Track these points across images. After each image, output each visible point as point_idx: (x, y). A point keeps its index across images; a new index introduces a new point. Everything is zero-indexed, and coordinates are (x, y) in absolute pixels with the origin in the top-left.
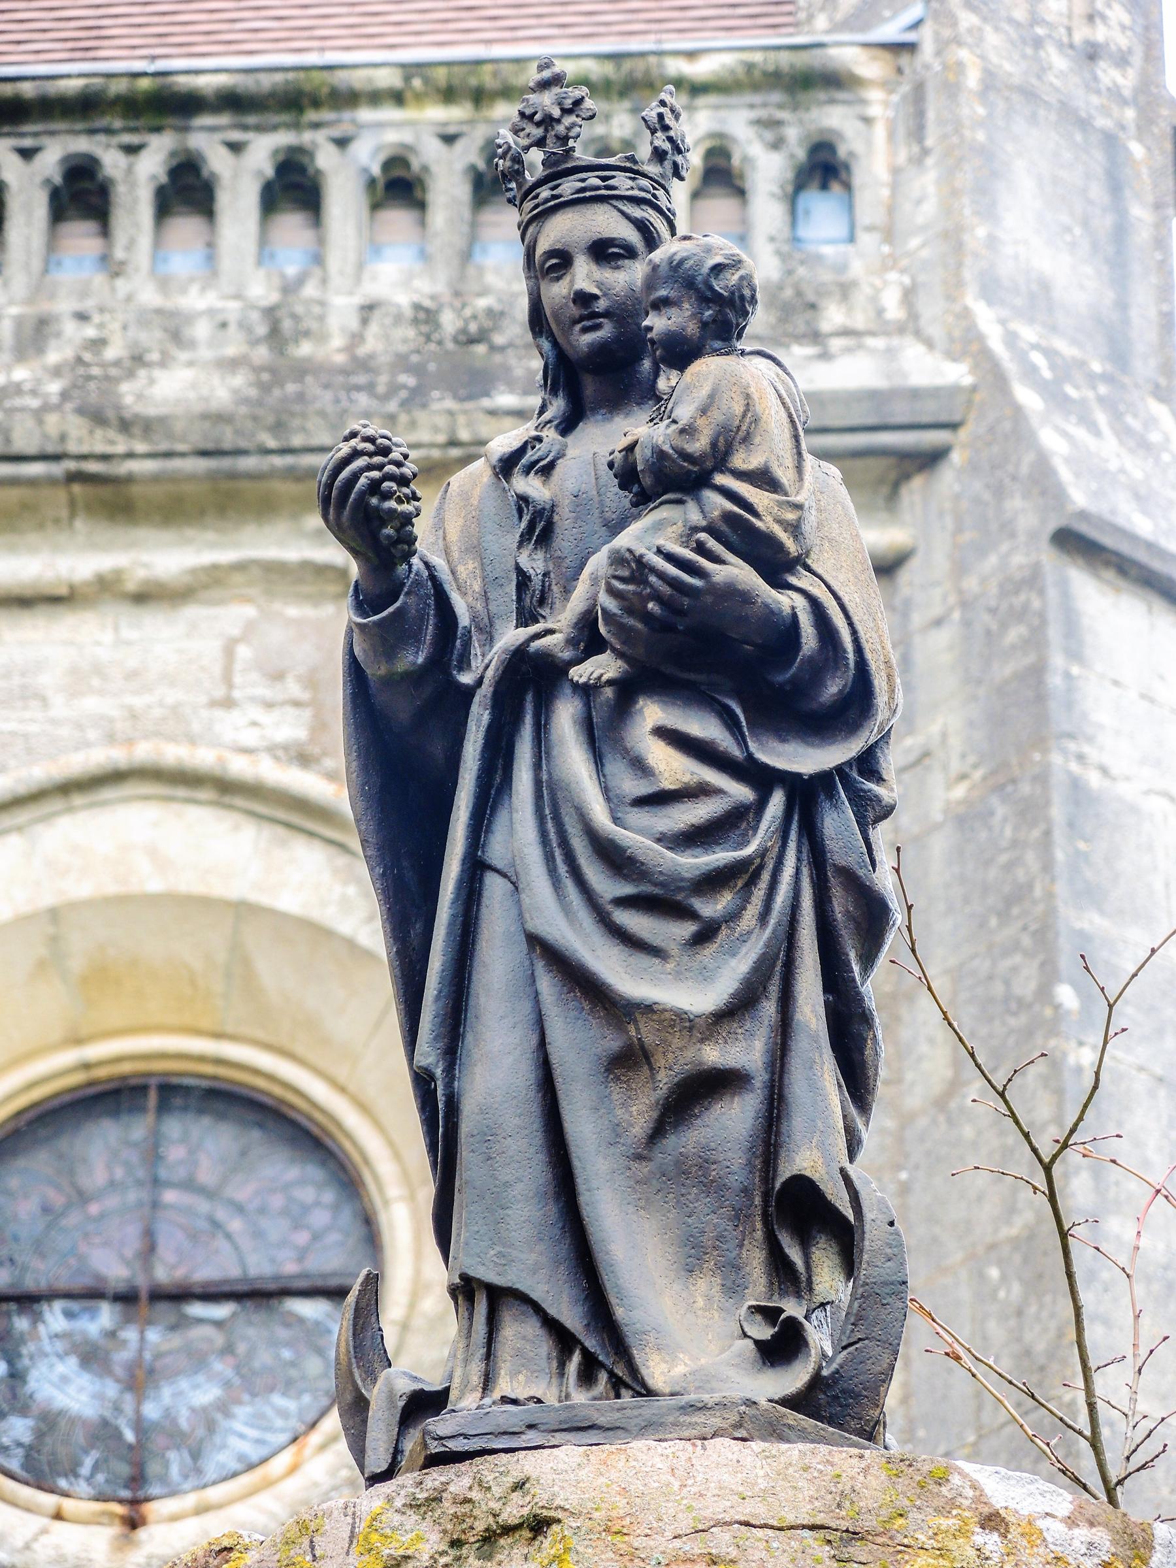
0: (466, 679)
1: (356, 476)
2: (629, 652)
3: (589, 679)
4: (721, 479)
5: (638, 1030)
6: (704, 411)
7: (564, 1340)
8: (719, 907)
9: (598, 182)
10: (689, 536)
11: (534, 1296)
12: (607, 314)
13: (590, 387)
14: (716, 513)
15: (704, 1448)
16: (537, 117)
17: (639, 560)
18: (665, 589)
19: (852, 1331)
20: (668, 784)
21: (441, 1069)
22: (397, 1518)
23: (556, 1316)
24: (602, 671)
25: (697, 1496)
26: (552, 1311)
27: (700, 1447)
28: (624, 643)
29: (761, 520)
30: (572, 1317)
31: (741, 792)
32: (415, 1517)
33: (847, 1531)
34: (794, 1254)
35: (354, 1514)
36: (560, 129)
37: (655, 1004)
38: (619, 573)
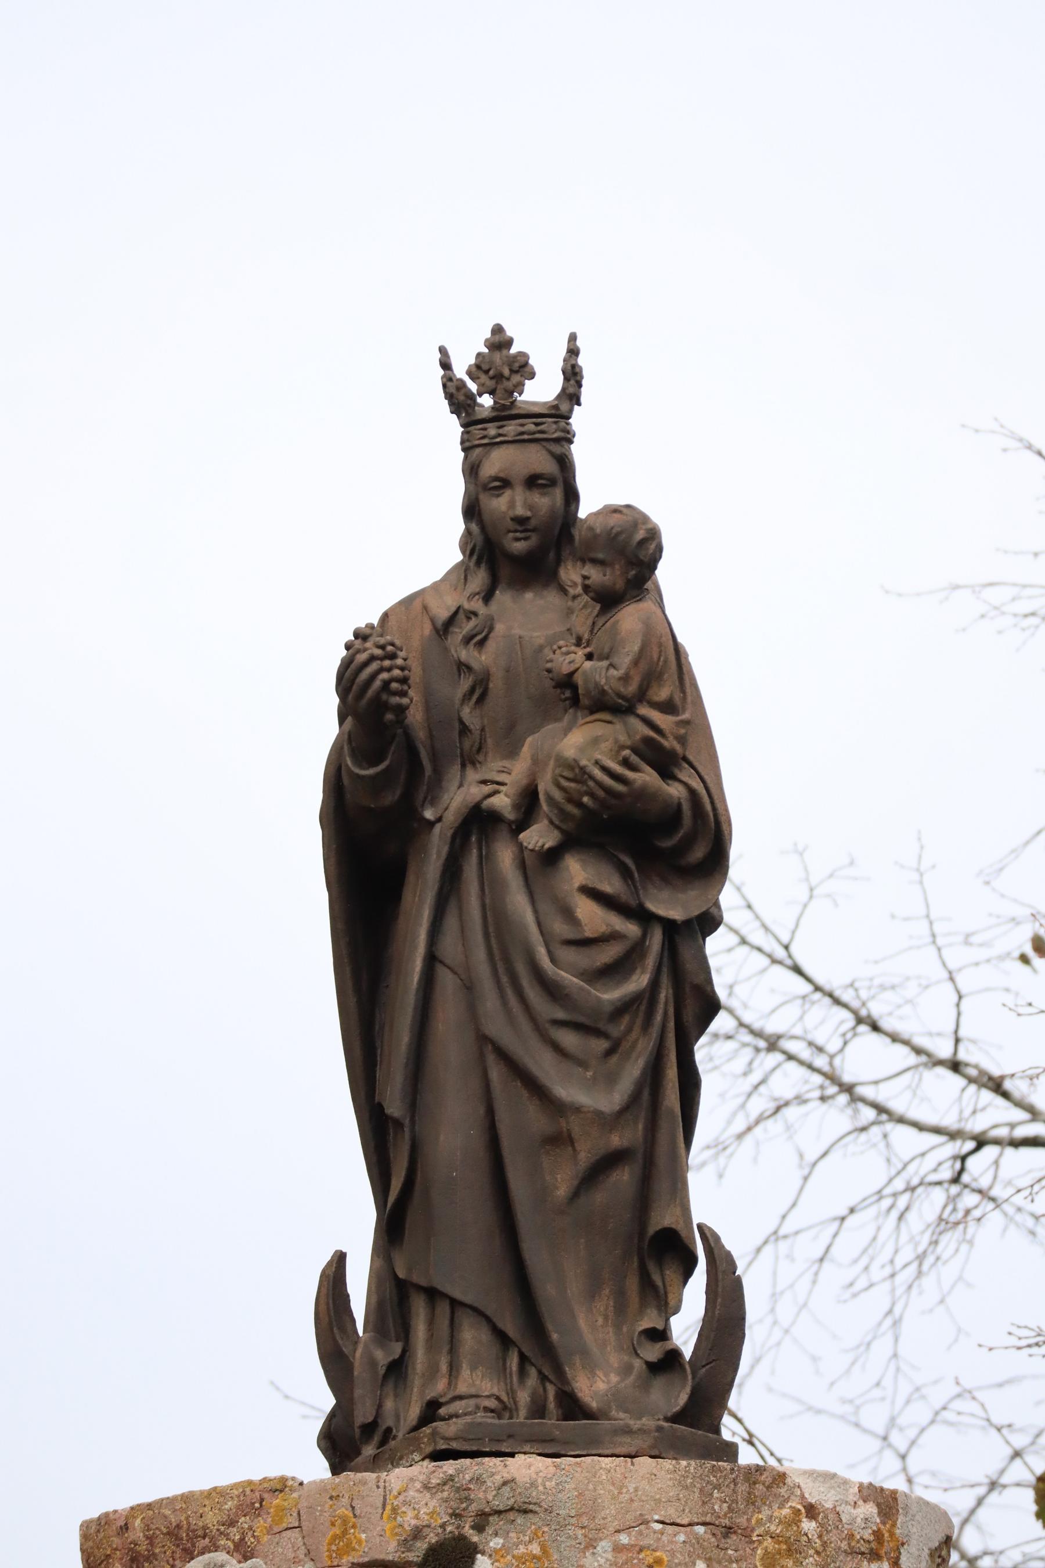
0: (429, 814)
1: (373, 677)
2: (564, 827)
3: (535, 846)
4: (644, 710)
5: (568, 1123)
6: (636, 663)
7: (504, 1340)
8: (622, 1028)
9: (532, 427)
10: (618, 752)
11: (488, 1313)
12: (533, 530)
13: (505, 571)
14: (638, 737)
15: (633, 1464)
16: (491, 373)
17: (583, 769)
18: (601, 793)
19: (709, 1354)
20: (588, 934)
21: (408, 1119)
22: (416, 1495)
23: (503, 1328)
24: (545, 840)
25: (629, 1501)
26: (500, 1325)
27: (630, 1464)
28: (562, 821)
29: (667, 740)
30: (511, 1329)
31: (631, 929)
32: (428, 1495)
33: (725, 1527)
34: (657, 1278)
35: (385, 1487)
36: (509, 385)
37: (582, 1107)
38: (565, 774)
